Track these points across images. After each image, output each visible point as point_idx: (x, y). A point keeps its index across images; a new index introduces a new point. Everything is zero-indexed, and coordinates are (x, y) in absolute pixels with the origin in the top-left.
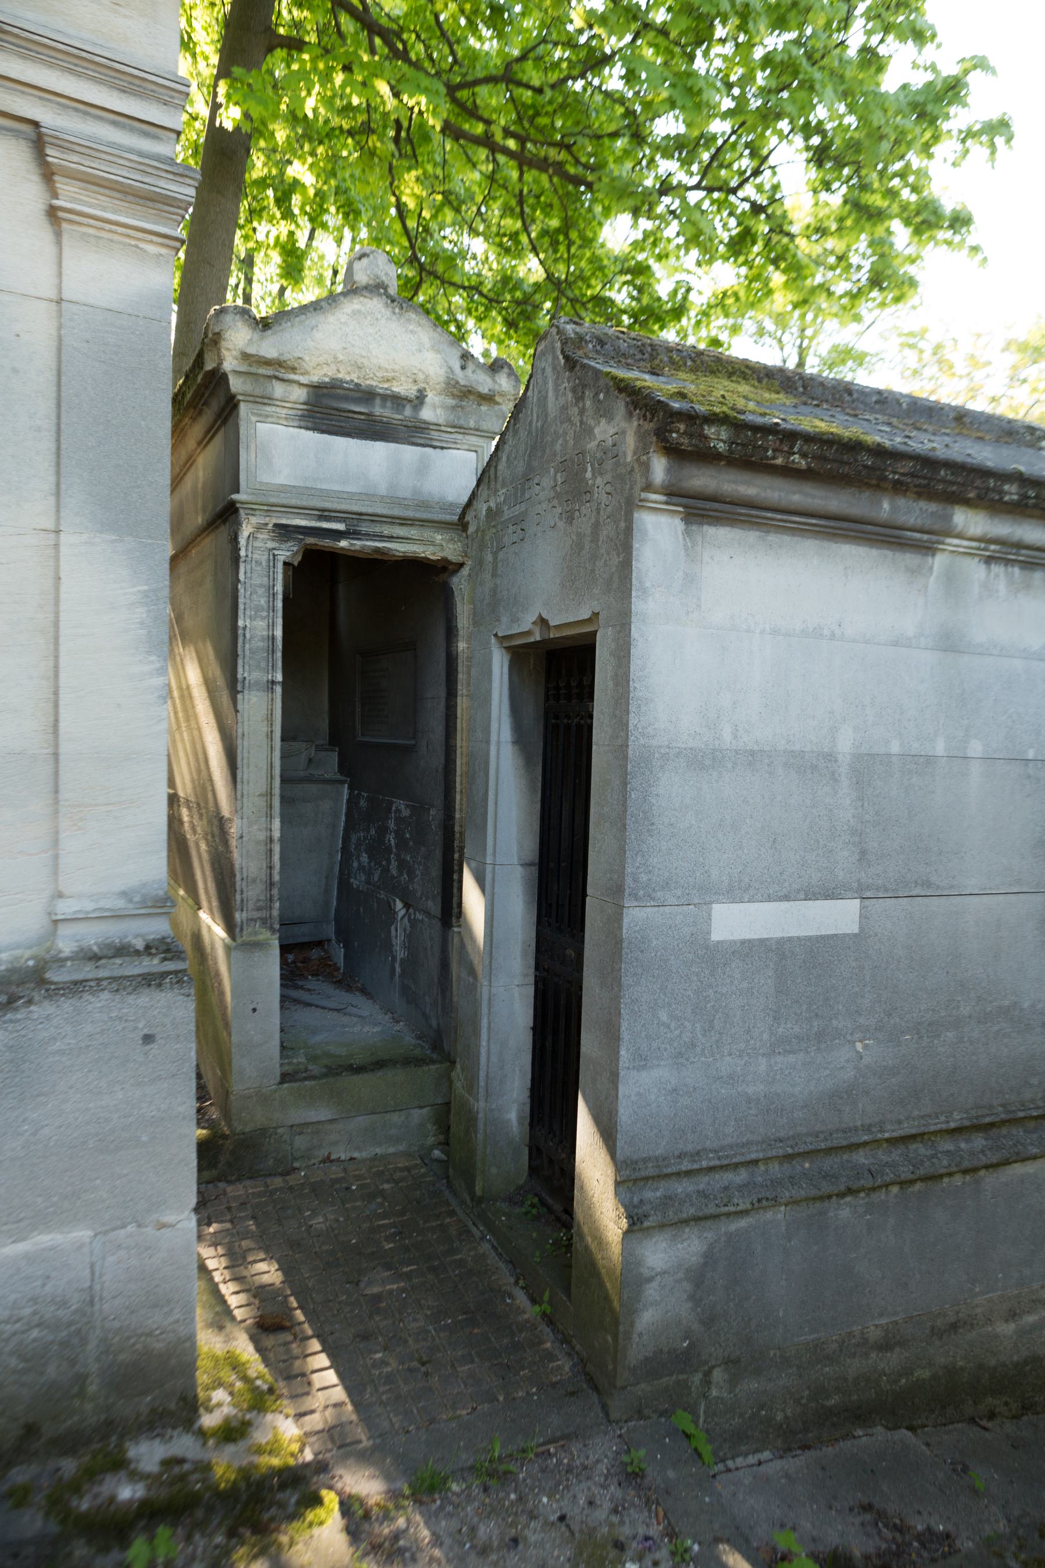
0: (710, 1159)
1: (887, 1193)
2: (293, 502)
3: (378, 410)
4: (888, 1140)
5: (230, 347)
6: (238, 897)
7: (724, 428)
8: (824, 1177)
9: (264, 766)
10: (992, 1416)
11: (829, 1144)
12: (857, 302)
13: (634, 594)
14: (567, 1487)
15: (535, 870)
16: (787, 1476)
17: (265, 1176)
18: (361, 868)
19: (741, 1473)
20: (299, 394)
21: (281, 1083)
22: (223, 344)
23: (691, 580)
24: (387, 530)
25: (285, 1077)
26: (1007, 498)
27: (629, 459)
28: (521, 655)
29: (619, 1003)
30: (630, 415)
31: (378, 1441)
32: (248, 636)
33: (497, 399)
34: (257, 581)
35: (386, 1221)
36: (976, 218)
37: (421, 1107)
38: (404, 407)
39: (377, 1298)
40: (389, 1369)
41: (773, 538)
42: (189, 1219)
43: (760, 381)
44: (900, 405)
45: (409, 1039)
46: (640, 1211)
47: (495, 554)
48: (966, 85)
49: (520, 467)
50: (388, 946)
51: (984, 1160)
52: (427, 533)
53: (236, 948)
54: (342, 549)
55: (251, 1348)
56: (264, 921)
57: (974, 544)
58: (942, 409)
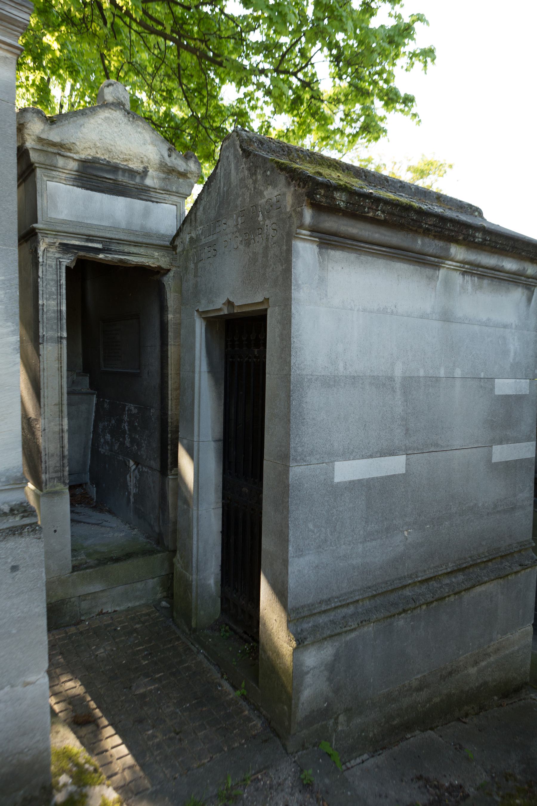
0: (336, 602)
1: (421, 610)
2: (71, 230)
3: (120, 178)
4: (419, 582)
5: (30, 133)
6: (43, 465)
7: (344, 193)
8: (392, 605)
9: (57, 387)
10: (467, 715)
11: (393, 587)
12: (356, 139)
13: (293, 288)
14: (271, 798)
15: (221, 443)
16: (378, 767)
17: (64, 627)
18: (106, 442)
19: (354, 769)
20: (73, 165)
21: (73, 571)
22: (26, 131)
23: (322, 280)
24: (126, 249)
25: (75, 568)
26: (476, 240)
27: (288, 210)
28: (213, 322)
29: (288, 521)
30: (289, 184)
31: (158, 787)
32: (45, 310)
33: (189, 175)
34: (50, 277)
35: (141, 647)
36: (416, 100)
37: (153, 578)
38: (135, 177)
39: (143, 696)
40: (158, 740)
41: (363, 258)
42: (44, 677)
43: (344, 171)
44: (411, 189)
45: (142, 539)
46: (302, 636)
47: (196, 264)
48: (413, 29)
49: (212, 214)
50: (125, 486)
51: (464, 587)
52: (150, 252)
53: (43, 495)
54: (100, 259)
55: (78, 743)
56: (59, 479)
57: (458, 264)
58: (430, 192)
